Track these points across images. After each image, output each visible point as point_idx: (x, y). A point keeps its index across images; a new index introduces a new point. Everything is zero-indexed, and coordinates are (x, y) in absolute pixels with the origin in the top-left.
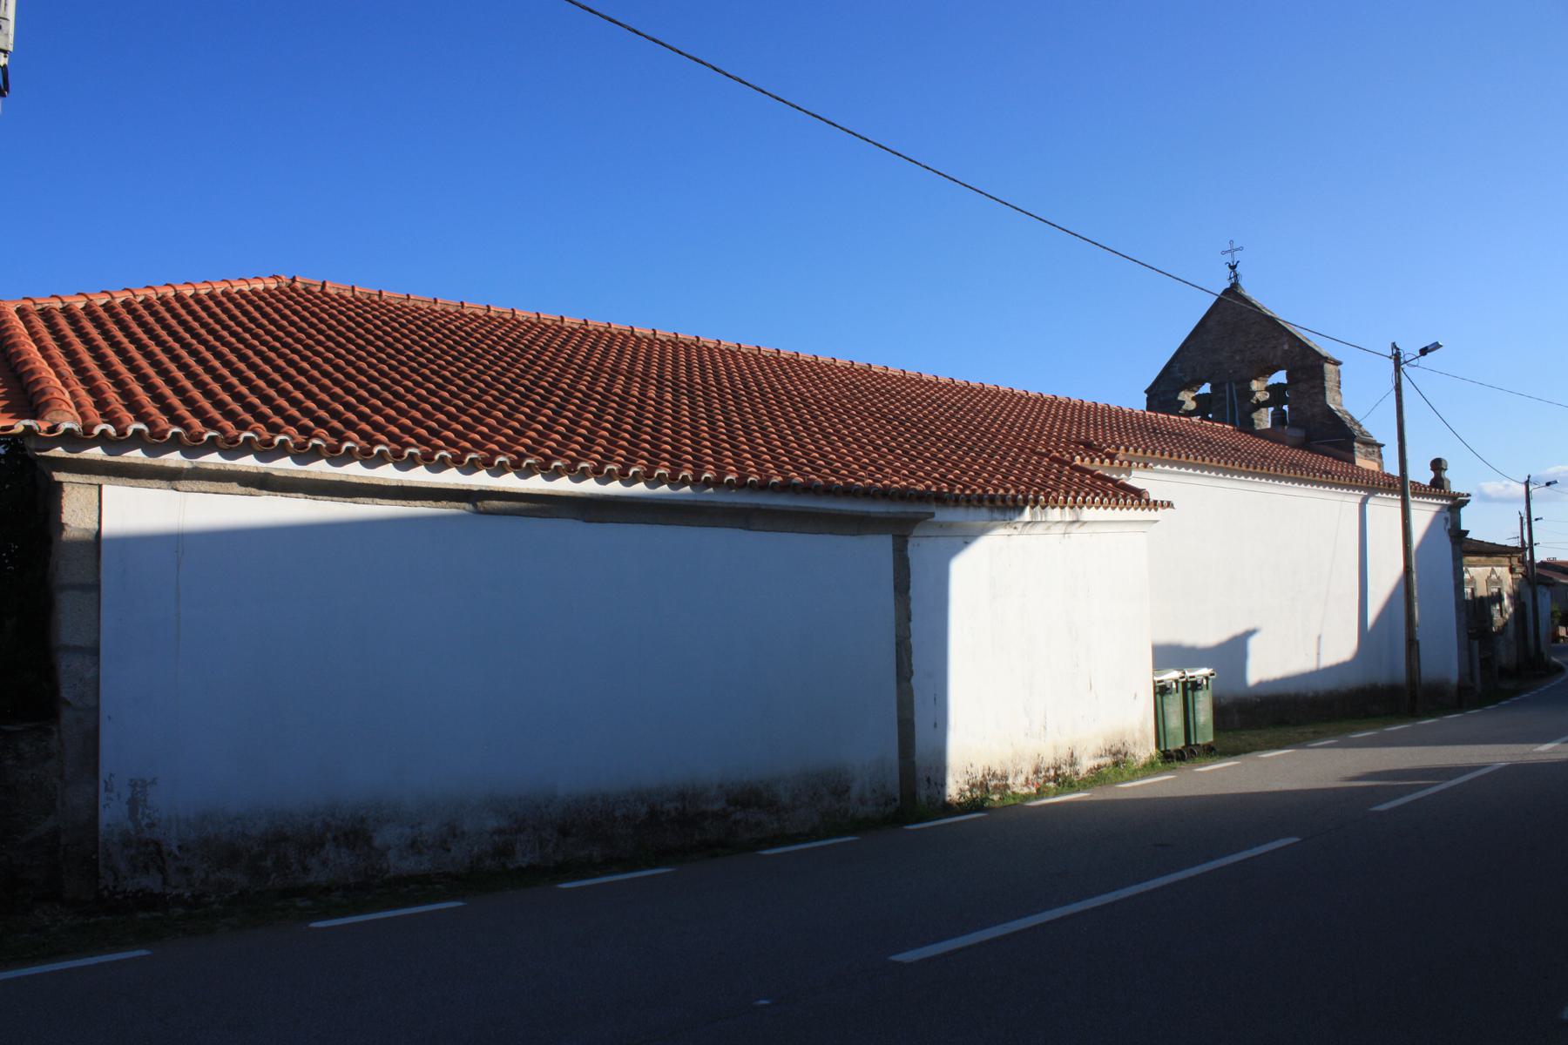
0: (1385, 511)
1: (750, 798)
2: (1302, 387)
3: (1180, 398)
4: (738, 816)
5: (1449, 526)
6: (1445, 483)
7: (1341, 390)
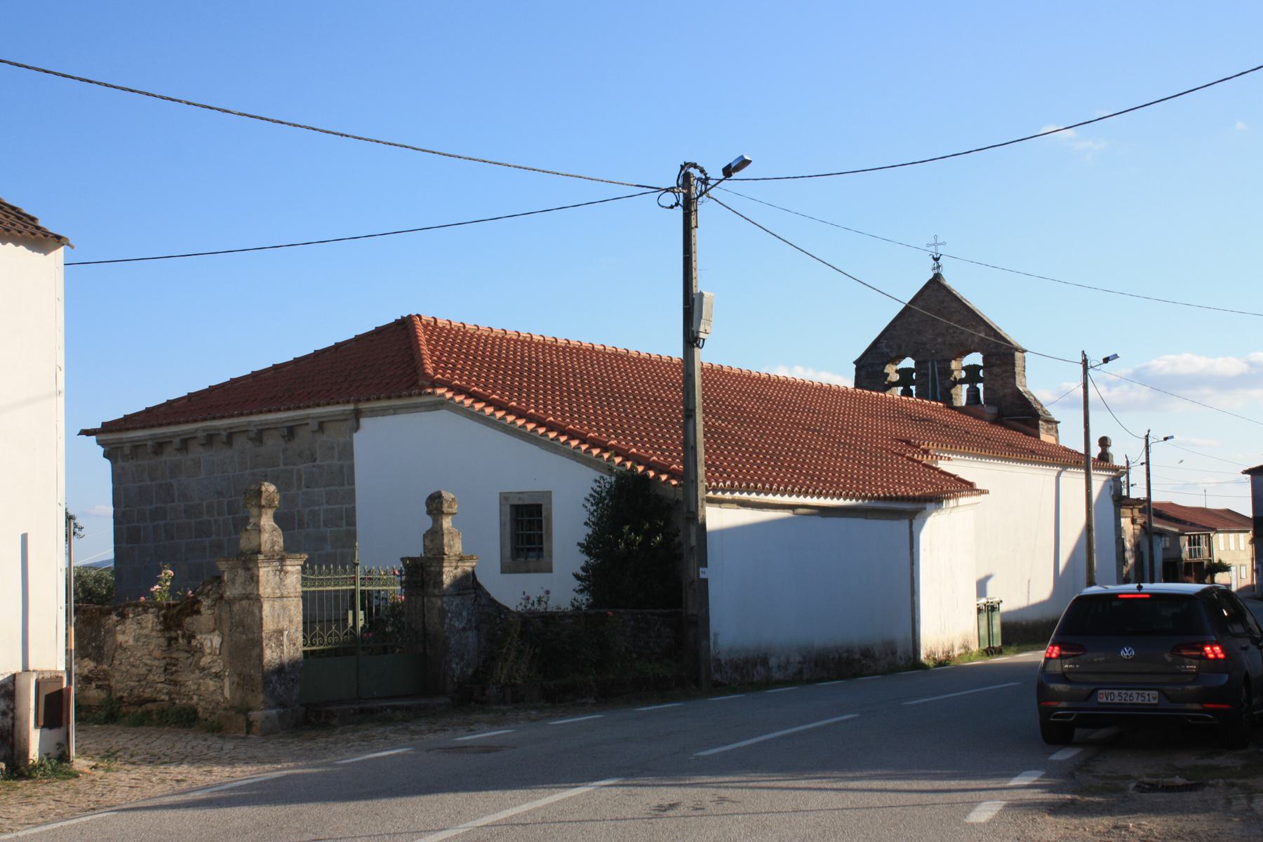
0: (1073, 481)
1: (867, 653)
2: (996, 370)
3: (886, 371)
4: (864, 662)
5: (1112, 493)
6: (1110, 457)
7: (1026, 373)
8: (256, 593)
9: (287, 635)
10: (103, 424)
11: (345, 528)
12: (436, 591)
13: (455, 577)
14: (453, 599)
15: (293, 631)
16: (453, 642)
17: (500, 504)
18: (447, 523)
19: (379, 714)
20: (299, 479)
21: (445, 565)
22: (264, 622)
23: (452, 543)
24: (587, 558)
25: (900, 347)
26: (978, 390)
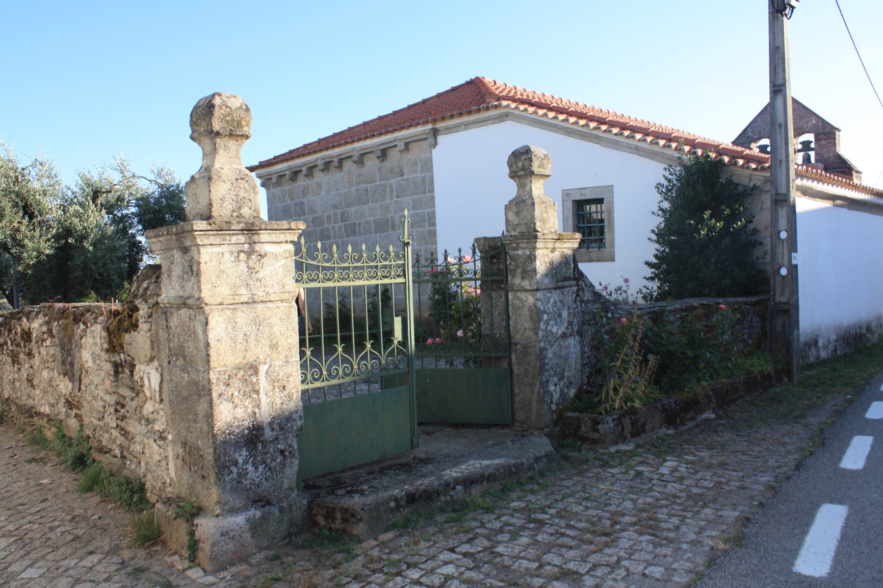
2: (823, 142)
8: (196, 296)
9: (267, 373)
10: (260, 162)
11: (427, 228)
12: (526, 284)
13: (552, 263)
14: (549, 295)
15: (278, 363)
16: (550, 355)
17: (563, 200)
18: (537, 188)
19: (443, 498)
20: (392, 191)
21: (538, 245)
22: (212, 352)
23: (545, 216)
24: (657, 246)
25: (760, 132)
26: (809, 156)
